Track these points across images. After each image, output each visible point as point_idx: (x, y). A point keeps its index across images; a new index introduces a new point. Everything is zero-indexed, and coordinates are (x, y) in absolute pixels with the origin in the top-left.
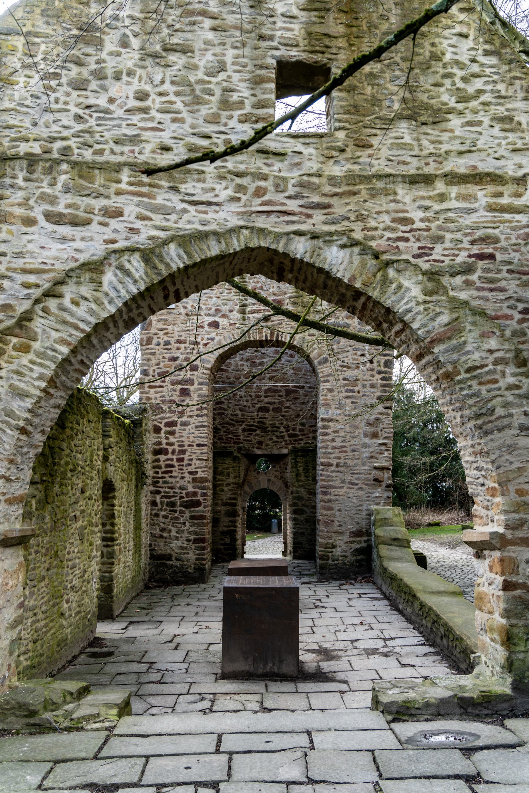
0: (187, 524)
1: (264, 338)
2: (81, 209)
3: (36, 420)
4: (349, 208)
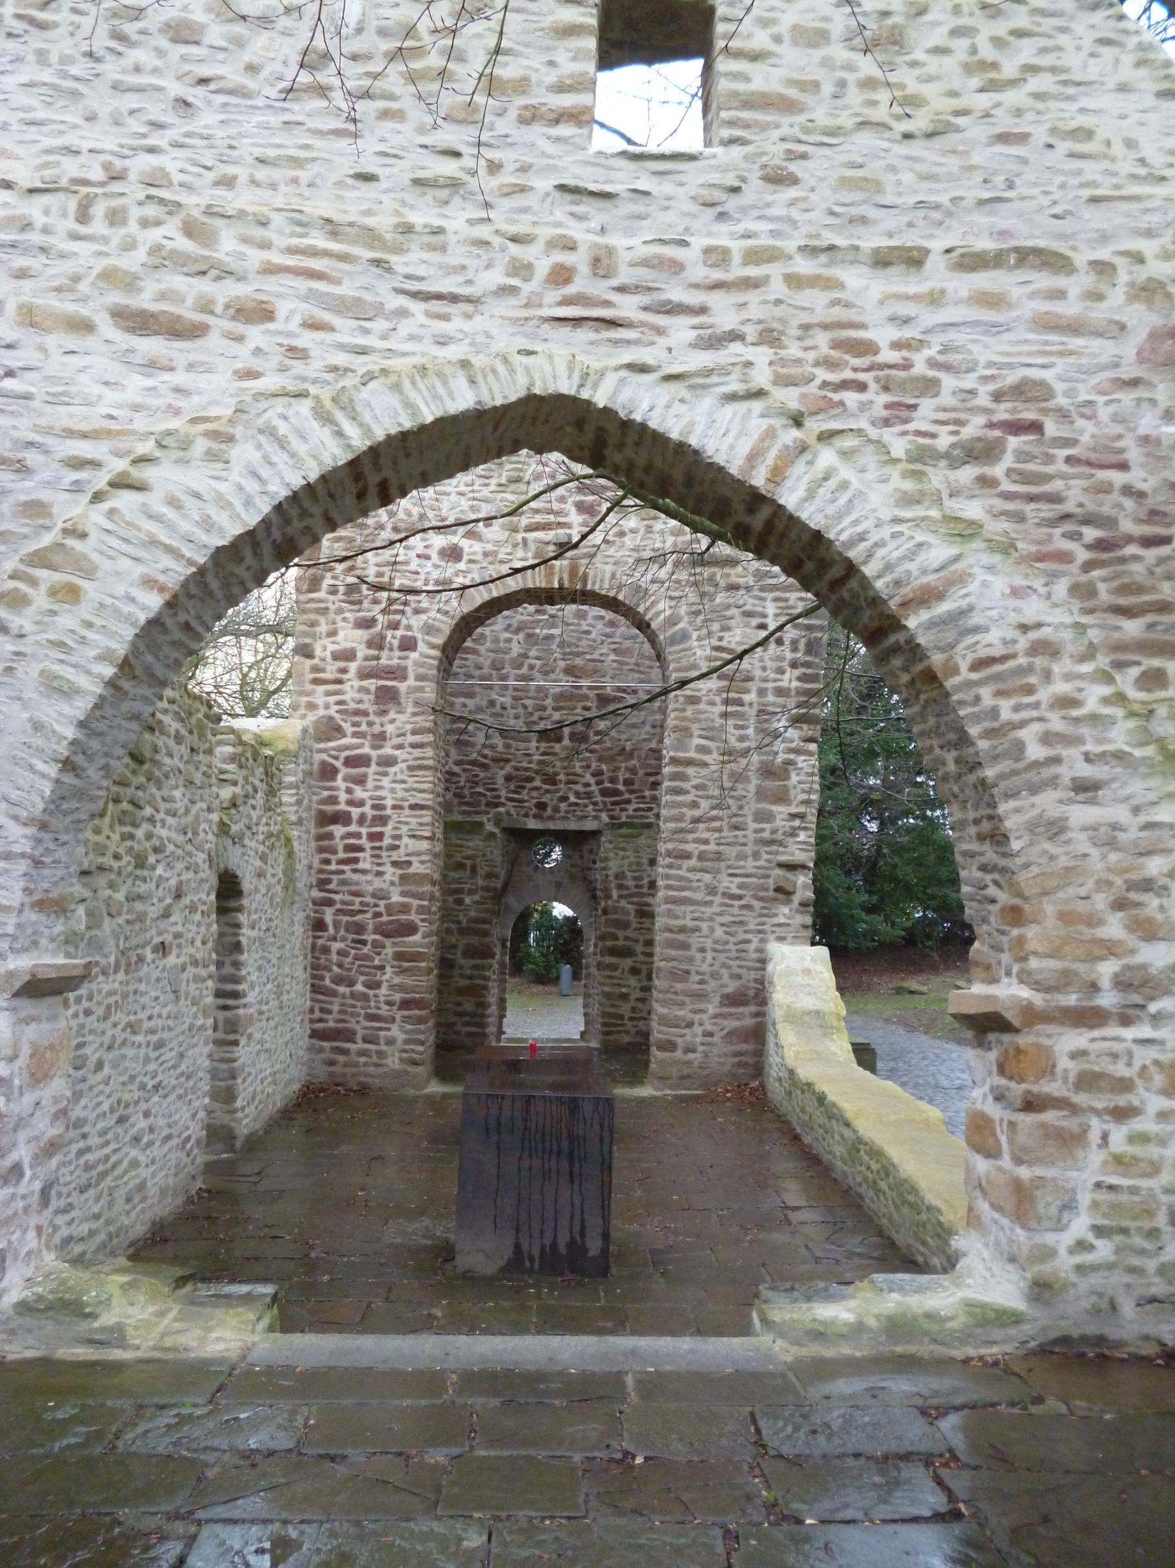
0: (388, 969)
1: (556, 585)
2: (189, 302)
3: (95, 744)
4: (745, 315)
